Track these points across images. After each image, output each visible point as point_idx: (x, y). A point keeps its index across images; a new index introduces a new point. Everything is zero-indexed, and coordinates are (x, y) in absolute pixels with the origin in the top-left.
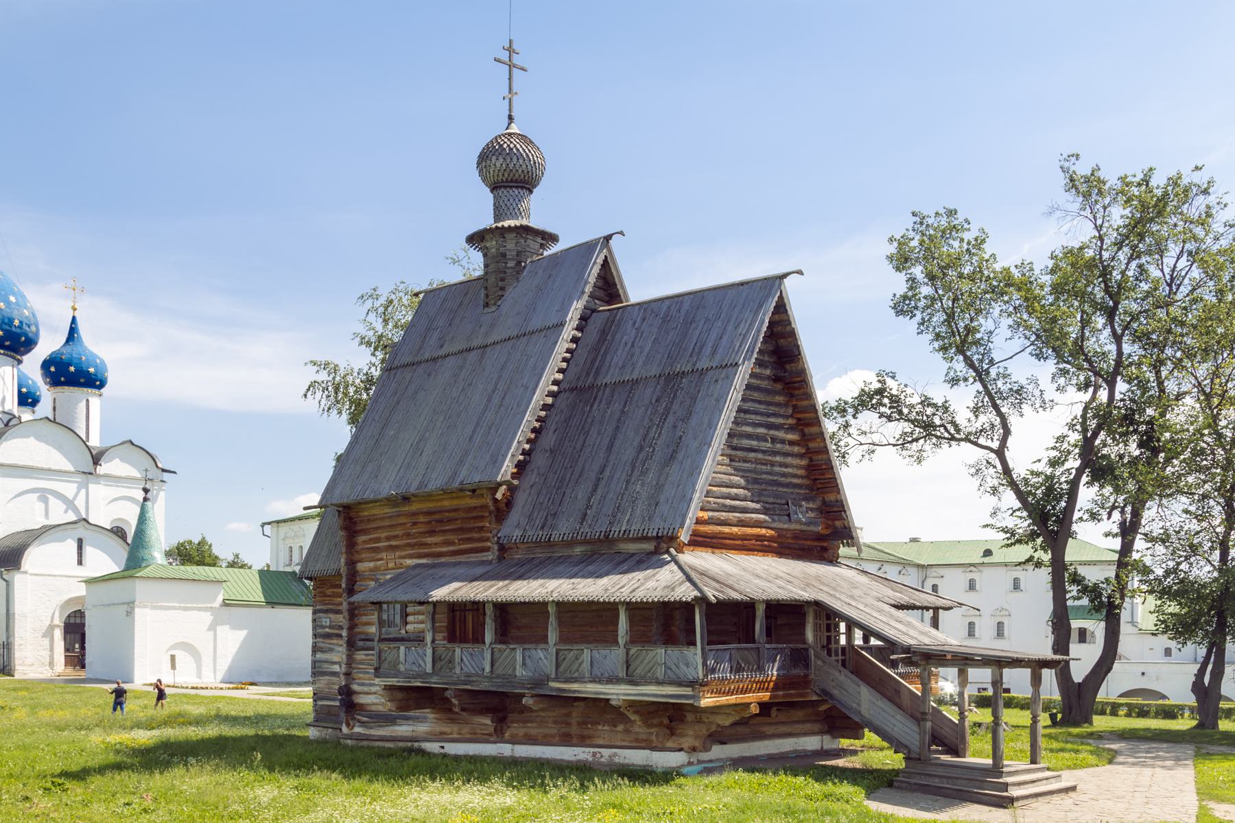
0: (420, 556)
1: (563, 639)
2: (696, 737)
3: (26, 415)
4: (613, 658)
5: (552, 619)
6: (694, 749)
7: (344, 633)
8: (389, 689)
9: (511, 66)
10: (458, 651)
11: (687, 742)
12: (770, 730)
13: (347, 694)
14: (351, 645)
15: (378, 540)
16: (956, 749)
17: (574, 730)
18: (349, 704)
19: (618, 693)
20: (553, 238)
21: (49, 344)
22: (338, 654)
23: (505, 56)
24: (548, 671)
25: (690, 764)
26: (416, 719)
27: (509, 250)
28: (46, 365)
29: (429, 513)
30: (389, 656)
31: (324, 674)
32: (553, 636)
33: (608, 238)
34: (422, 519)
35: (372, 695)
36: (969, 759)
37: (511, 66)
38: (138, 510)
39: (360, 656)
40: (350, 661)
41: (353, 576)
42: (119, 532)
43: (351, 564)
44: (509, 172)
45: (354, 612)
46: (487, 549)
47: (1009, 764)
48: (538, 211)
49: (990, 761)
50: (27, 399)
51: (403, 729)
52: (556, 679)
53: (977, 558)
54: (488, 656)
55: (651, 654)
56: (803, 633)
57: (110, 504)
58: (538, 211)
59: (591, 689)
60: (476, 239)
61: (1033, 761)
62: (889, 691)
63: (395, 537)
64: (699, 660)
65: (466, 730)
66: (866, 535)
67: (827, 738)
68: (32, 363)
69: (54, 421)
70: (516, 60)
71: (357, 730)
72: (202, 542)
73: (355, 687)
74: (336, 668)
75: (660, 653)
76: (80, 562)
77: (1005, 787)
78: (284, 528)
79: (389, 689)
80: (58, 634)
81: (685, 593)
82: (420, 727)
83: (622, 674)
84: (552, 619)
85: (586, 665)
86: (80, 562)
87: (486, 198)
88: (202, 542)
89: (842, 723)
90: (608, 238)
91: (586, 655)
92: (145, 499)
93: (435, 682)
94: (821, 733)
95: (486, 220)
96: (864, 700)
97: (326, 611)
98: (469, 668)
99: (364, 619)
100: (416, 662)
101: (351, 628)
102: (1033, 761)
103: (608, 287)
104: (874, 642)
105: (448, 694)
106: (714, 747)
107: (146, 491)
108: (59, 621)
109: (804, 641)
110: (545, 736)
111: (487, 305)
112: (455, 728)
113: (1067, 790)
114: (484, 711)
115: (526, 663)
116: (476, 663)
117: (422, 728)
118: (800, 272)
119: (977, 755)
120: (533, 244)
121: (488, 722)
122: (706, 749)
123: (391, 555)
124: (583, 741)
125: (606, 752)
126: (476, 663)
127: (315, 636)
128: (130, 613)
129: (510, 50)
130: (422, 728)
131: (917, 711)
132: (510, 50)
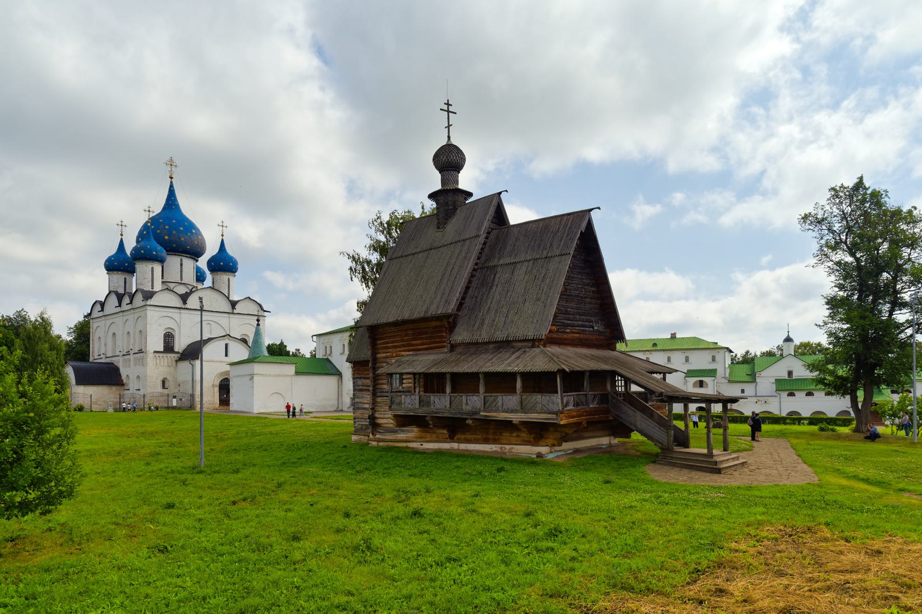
0: (409, 351)
1: (453, 391)
2: (555, 439)
3: (200, 286)
4: (512, 400)
5: (482, 381)
6: (554, 445)
7: (371, 389)
8: (396, 416)
9: (448, 111)
10: (432, 398)
11: (550, 441)
12: (587, 435)
13: (372, 418)
14: (374, 395)
15: (387, 343)
16: (686, 445)
17: (490, 437)
18: (374, 425)
19: (516, 417)
20: (470, 194)
21: (211, 250)
22: (367, 398)
23: (445, 107)
24: (478, 407)
25: (551, 452)
26: (408, 431)
27: (449, 198)
28: (209, 263)
29: (414, 329)
30: (397, 400)
31: (359, 408)
32: (448, 390)
33: (500, 193)
34: (410, 332)
35: (386, 419)
36: (691, 450)
37: (448, 111)
38: (254, 330)
39: (379, 399)
40: (374, 403)
41: (375, 360)
42: (244, 341)
43: (374, 353)
44: (449, 160)
45: (376, 379)
46: (444, 347)
47: (715, 452)
48: (466, 180)
49: (705, 451)
50: (200, 278)
51: (401, 436)
52: (484, 411)
53: (649, 347)
54: (448, 399)
55: (534, 398)
56: (606, 386)
57: (242, 327)
58: (466, 180)
59: (502, 416)
60: (432, 196)
61: (725, 450)
62: (649, 413)
63: (397, 341)
64: (559, 401)
65: (434, 436)
66: (628, 336)
67: (612, 438)
68: (203, 262)
69: (212, 288)
70: (451, 109)
71: (377, 436)
72: (282, 343)
73: (377, 415)
74: (367, 406)
75: (538, 398)
76: (226, 355)
77: (716, 463)
78: (322, 338)
79: (396, 416)
80: (217, 389)
81: (553, 368)
82: (409, 436)
83: (519, 408)
84: (482, 381)
85: (500, 403)
86: (226, 355)
87: (437, 176)
88: (282, 343)
89: (623, 430)
90: (500, 193)
91: (500, 398)
92: (258, 325)
93: (421, 412)
94: (609, 435)
95: (438, 186)
96: (638, 418)
97: (360, 378)
98: (438, 406)
99: (381, 382)
100: (410, 403)
101: (374, 386)
102: (725, 450)
103: (500, 215)
104: (634, 388)
105: (428, 418)
106: (564, 444)
107: (258, 320)
108: (217, 383)
109: (606, 389)
110: (475, 439)
111: (438, 228)
112: (428, 435)
113: (743, 463)
114: (443, 427)
115: (472, 402)
116: (441, 403)
117: (411, 435)
118: (599, 208)
119: (697, 448)
120: (461, 198)
121: (445, 432)
122: (560, 445)
123: (394, 350)
124: (495, 441)
125: (508, 447)
126: (441, 403)
127: (354, 390)
128: (252, 379)
129: (448, 104)
130: (411, 435)
131: (664, 424)
132: (448, 104)
